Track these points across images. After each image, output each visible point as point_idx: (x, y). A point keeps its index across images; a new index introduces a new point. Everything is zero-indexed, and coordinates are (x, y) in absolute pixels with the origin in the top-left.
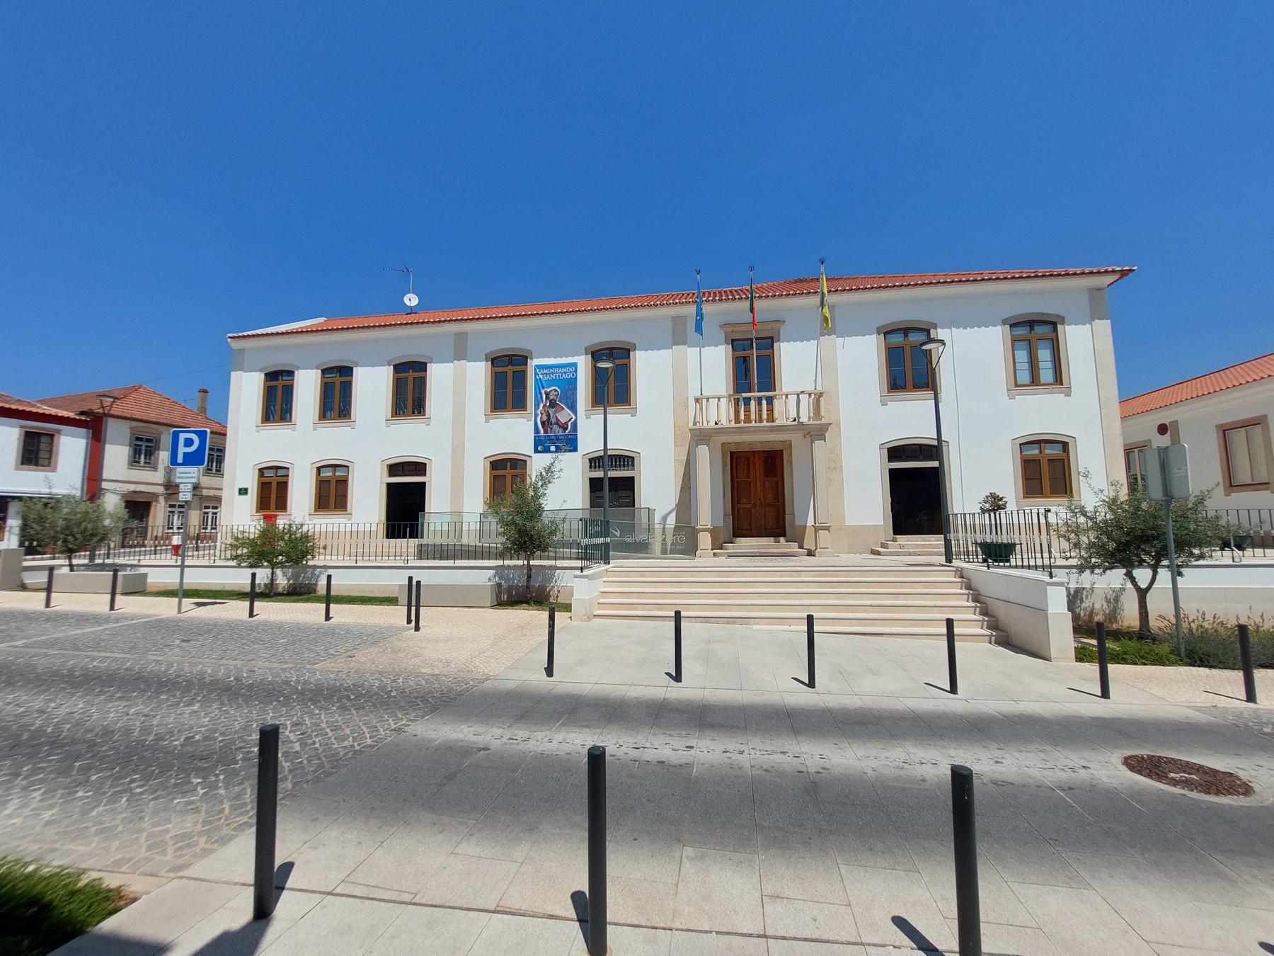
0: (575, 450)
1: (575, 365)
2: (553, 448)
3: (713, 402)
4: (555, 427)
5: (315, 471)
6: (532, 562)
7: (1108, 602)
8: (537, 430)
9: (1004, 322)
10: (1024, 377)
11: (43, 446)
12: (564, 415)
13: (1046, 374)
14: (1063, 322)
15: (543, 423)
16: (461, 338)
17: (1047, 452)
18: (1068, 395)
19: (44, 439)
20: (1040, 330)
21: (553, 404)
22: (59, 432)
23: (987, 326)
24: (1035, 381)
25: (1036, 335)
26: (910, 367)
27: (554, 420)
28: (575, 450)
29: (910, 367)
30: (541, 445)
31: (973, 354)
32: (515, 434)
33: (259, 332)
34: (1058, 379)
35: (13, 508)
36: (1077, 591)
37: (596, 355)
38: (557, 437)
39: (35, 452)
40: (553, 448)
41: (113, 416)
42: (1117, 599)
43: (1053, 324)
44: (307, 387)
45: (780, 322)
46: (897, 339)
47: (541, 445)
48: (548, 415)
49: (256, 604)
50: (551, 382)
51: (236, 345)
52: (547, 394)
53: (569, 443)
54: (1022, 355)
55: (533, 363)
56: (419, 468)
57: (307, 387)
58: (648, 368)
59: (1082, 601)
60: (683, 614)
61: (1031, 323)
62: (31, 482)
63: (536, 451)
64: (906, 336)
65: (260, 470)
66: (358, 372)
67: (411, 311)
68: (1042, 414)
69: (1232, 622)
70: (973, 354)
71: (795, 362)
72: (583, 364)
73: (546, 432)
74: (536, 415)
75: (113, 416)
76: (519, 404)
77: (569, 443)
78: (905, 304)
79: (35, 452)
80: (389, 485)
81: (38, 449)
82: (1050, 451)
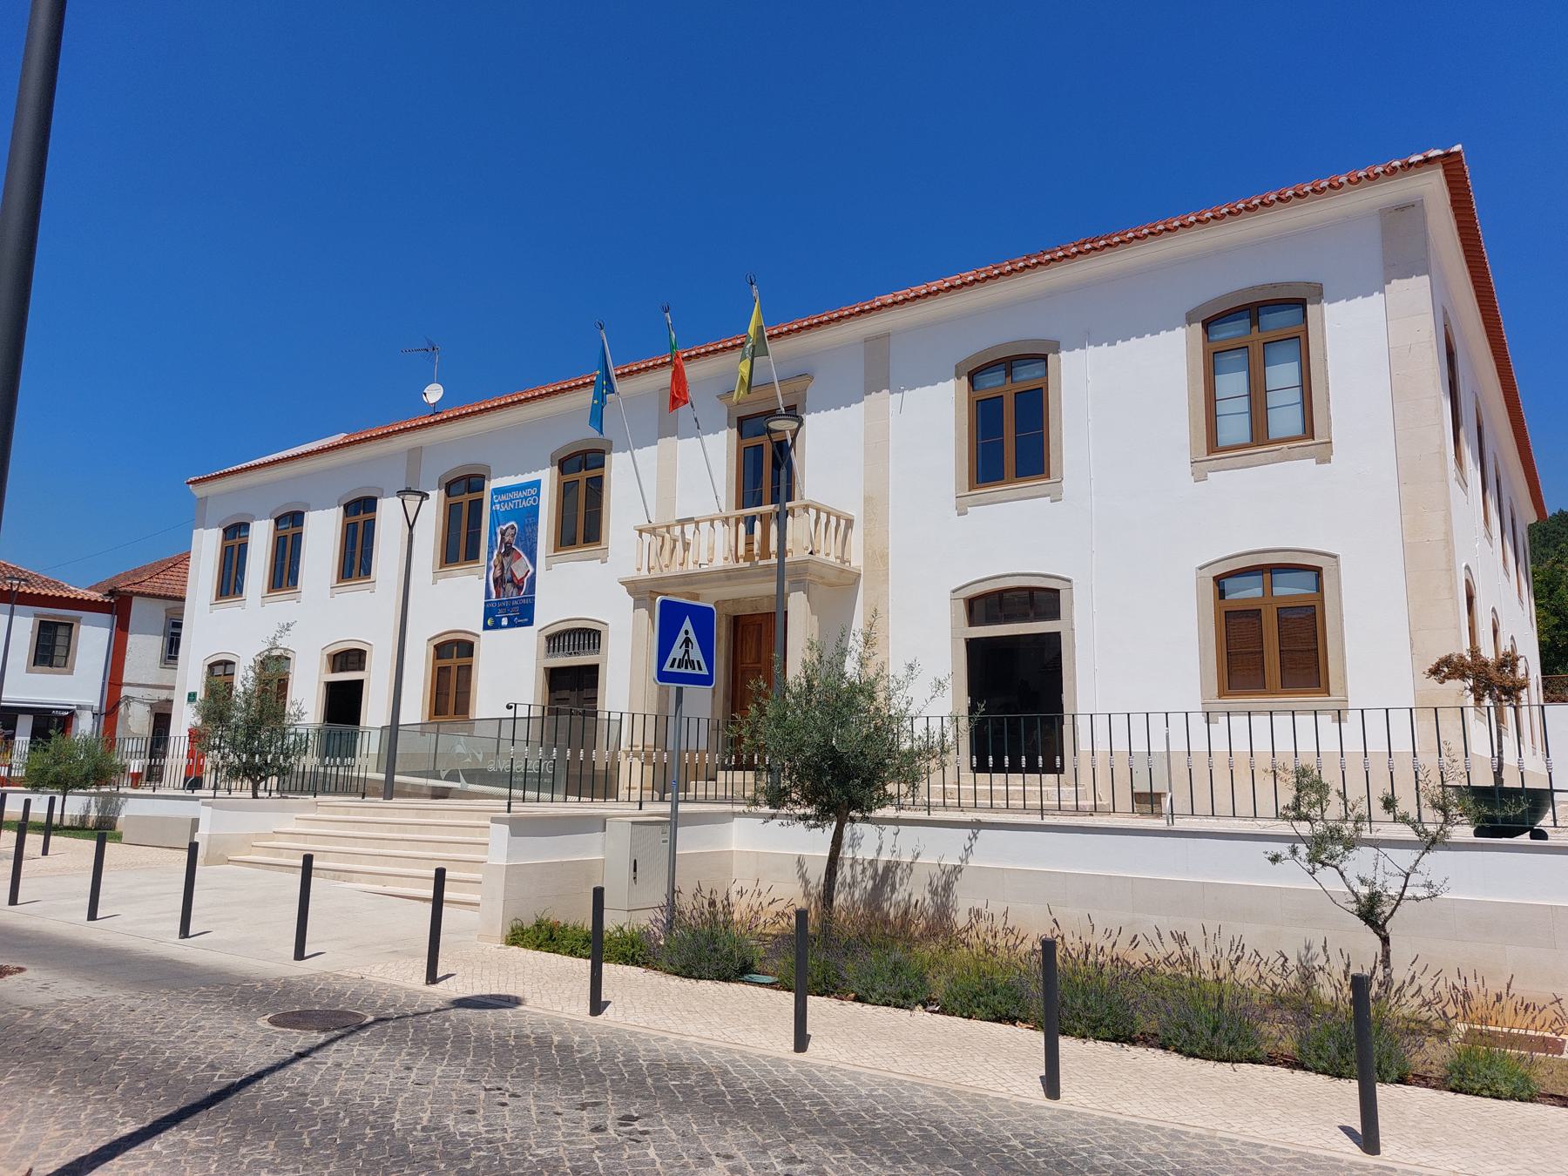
0: (530, 623)
1: (539, 482)
2: (505, 622)
3: (705, 526)
4: (509, 586)
5: (1210, 586)
6: (682, 808)
7: (934, 893)
8: (488, 595)
9: (1190, 320)
10: (1235, 427)
11: (60, 641)
12: (520, 568)
13: (1284, 419)
14: (1318, 293)
15: (495, 581)
16: (877, 346)
17: (1279, 591)
18: (1324, 459)
19: (62, 631)
20: (1275, 322)
21: (509, 551)
22: (78, 620)
23: (1155, 332)
24: (1260, 435)
25: (1257, 332)
26: (1010, 438)
27: (507, 576)
28: (530, 623)
29: (1010, 438)
30: (492, 618)
31: (1125, 391)
32: (457, 600)
33: (252, 463)
34: (1308, 431)
35: (25, 724)
36: (890, 868)
37: (566, 464)
38: (511, 606)
39: (50, 649)
40: (505, 622)
41: (142, 595)
42: (947, 887)
43: (1296, 303)
44: (323, 533)
45: (806, 376)
46: (994, 383)
47: (492, 618)
48: (502, 568)
49: (53, 839)
50: (509, 515)
51: (199, 491)
52: (503, 534)
53: (522, 614)
54: (1233, 383)
55: (492, 484)
56: (1041, 600)
57: (323, 533)
58: (628, 482)
59: (893, 890)
60: (448, 875)
61: (1252, 310)
62: (29, 687)
63: (486, 627)
64: (1009, 373)
65: (1218, 580)
66: (1426, 278)
67: (435, 409)
68: (1266, 507)
69: (1035, 928)
70: (1125, 391)
71: (827, 448)
72: (548, 478)
73: (498, 596)
74: (489, 569)
75: (142, 595)
76: (472, 555)
77: (522, 614)
78: (992, 311)
79: (50, 649)
80: (972, 644)
81: (54, 646)
82: (1288, 589)
